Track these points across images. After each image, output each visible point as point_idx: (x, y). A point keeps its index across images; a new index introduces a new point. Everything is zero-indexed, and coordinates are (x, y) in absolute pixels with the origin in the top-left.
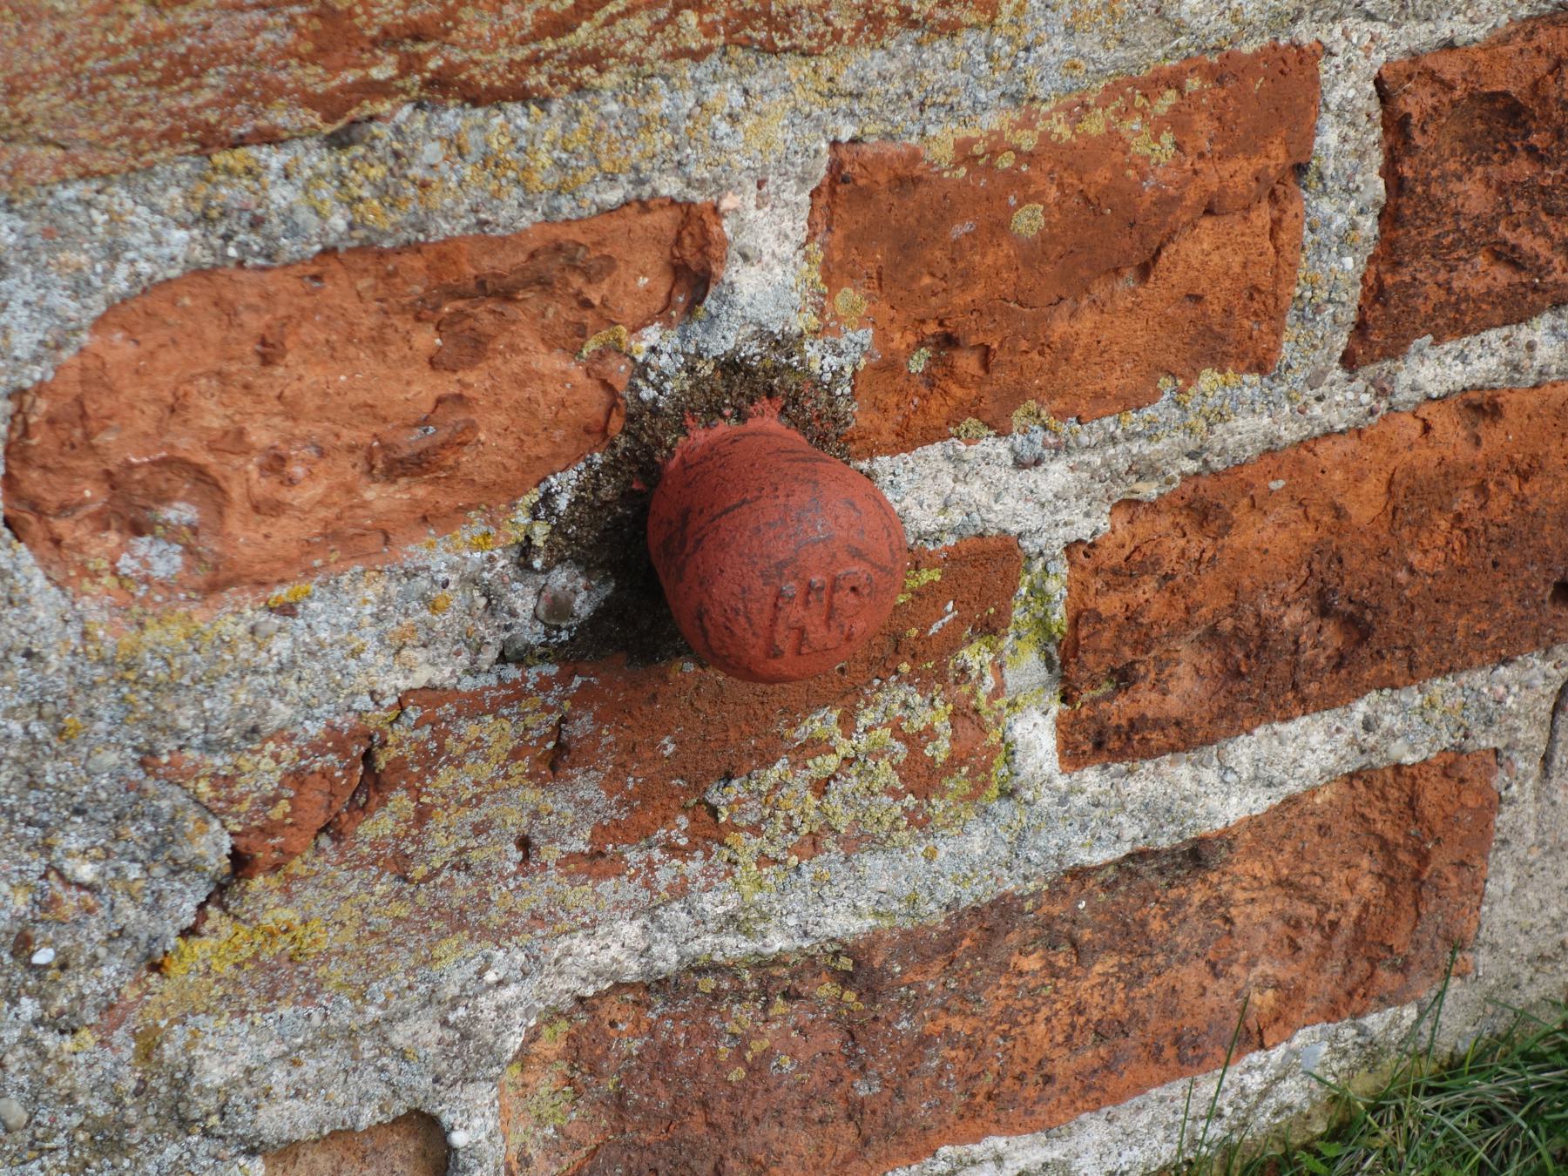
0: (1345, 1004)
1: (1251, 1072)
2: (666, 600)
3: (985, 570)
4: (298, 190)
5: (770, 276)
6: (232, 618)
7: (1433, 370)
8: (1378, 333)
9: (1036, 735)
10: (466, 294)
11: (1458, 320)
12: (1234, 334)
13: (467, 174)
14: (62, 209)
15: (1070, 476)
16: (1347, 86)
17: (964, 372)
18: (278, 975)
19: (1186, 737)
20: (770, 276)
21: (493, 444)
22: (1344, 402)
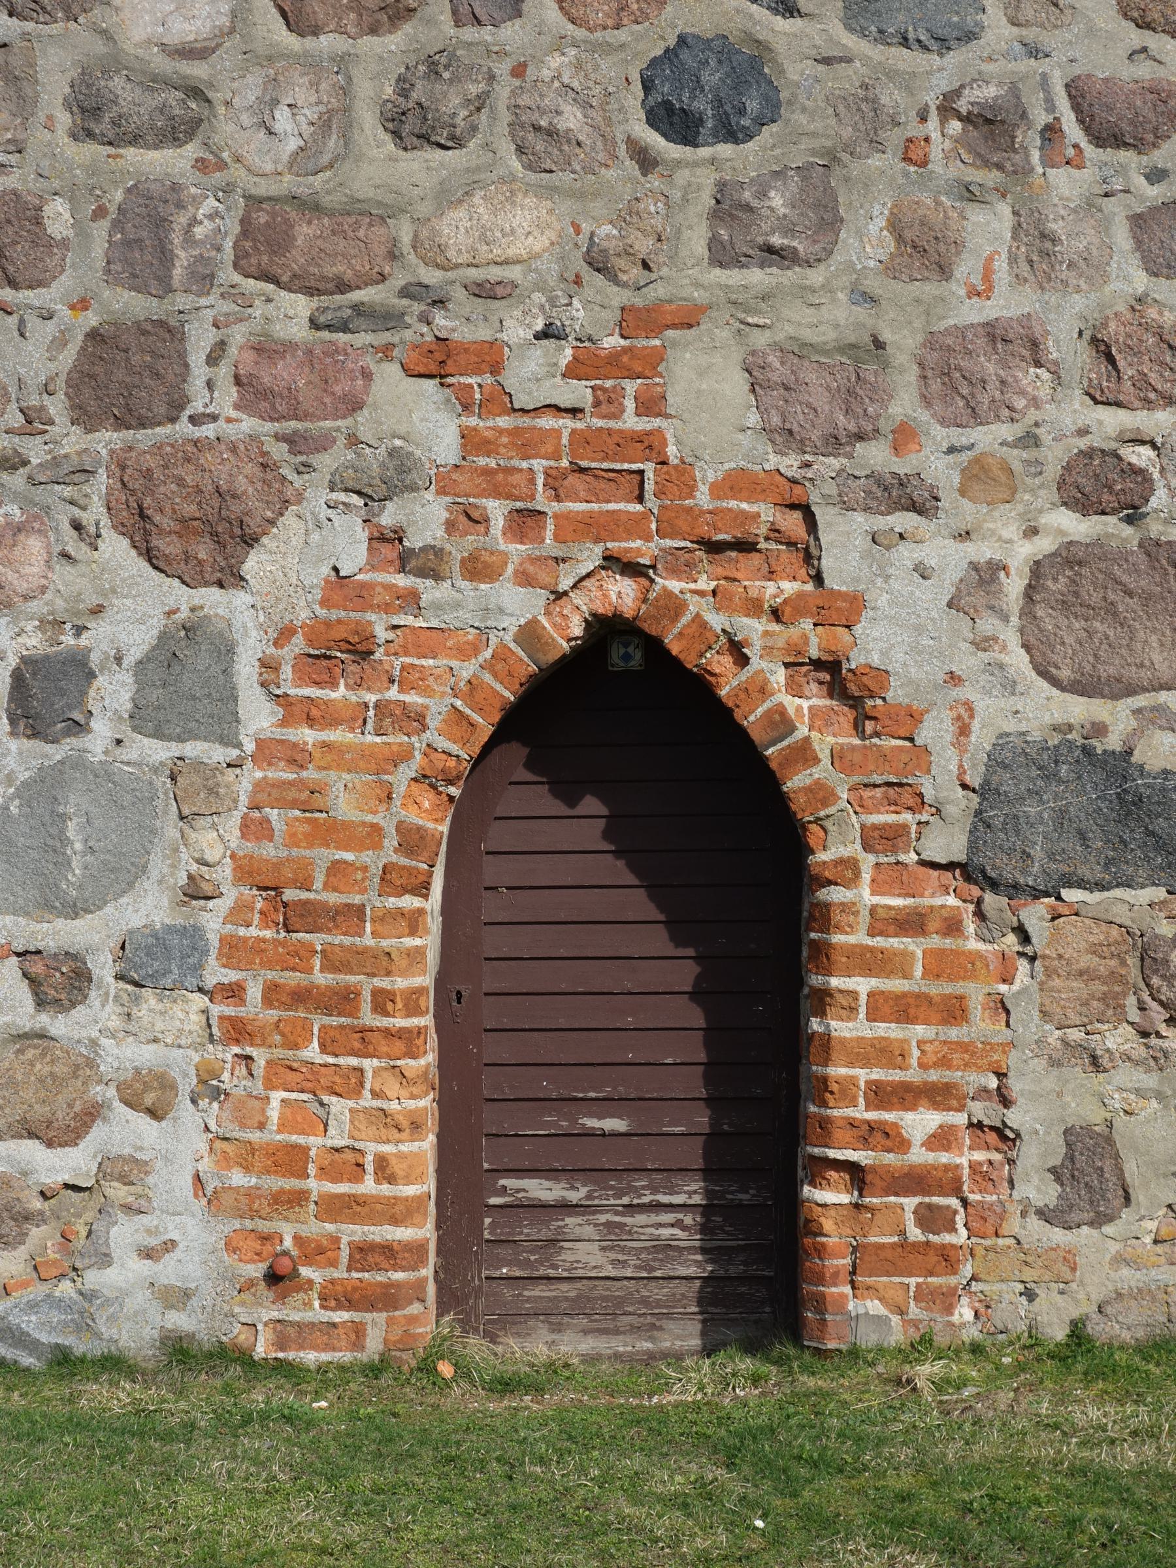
0: (352, 1351)
1: (285, 424)
2: (277, 1278)
3: (310, 1282)
4: (249, 1225)
5: (288, 1243)
6: (241, 1264)
7: (355, 1275)
8: (349, 1270)
9: (317, 1304)
10: (266, 1238)
11: (358, 1270)
12: (334, 1264)
13: (263, 1226)
14: (589, 1299)
15: (719, 631)
16: (862, 1016)
17: (308, 1260)
18: (243, 1304)
19: (333, 1310)
20: (288, 1243)
21: (265, 1255)
22: (345, 1275)
